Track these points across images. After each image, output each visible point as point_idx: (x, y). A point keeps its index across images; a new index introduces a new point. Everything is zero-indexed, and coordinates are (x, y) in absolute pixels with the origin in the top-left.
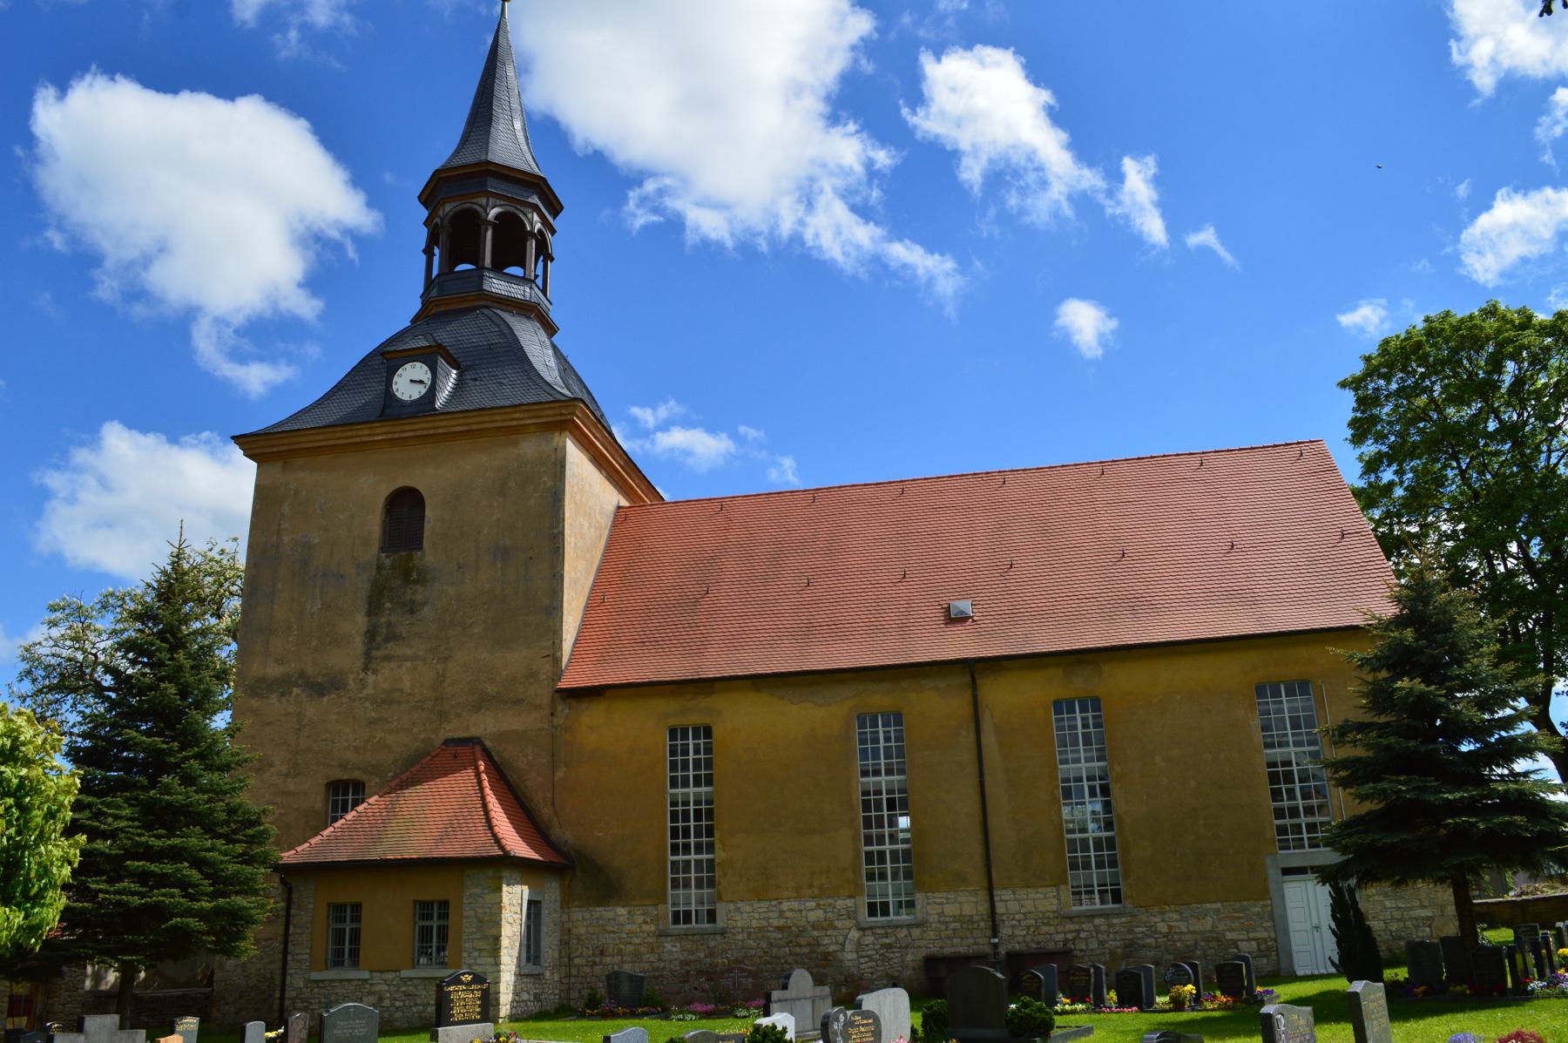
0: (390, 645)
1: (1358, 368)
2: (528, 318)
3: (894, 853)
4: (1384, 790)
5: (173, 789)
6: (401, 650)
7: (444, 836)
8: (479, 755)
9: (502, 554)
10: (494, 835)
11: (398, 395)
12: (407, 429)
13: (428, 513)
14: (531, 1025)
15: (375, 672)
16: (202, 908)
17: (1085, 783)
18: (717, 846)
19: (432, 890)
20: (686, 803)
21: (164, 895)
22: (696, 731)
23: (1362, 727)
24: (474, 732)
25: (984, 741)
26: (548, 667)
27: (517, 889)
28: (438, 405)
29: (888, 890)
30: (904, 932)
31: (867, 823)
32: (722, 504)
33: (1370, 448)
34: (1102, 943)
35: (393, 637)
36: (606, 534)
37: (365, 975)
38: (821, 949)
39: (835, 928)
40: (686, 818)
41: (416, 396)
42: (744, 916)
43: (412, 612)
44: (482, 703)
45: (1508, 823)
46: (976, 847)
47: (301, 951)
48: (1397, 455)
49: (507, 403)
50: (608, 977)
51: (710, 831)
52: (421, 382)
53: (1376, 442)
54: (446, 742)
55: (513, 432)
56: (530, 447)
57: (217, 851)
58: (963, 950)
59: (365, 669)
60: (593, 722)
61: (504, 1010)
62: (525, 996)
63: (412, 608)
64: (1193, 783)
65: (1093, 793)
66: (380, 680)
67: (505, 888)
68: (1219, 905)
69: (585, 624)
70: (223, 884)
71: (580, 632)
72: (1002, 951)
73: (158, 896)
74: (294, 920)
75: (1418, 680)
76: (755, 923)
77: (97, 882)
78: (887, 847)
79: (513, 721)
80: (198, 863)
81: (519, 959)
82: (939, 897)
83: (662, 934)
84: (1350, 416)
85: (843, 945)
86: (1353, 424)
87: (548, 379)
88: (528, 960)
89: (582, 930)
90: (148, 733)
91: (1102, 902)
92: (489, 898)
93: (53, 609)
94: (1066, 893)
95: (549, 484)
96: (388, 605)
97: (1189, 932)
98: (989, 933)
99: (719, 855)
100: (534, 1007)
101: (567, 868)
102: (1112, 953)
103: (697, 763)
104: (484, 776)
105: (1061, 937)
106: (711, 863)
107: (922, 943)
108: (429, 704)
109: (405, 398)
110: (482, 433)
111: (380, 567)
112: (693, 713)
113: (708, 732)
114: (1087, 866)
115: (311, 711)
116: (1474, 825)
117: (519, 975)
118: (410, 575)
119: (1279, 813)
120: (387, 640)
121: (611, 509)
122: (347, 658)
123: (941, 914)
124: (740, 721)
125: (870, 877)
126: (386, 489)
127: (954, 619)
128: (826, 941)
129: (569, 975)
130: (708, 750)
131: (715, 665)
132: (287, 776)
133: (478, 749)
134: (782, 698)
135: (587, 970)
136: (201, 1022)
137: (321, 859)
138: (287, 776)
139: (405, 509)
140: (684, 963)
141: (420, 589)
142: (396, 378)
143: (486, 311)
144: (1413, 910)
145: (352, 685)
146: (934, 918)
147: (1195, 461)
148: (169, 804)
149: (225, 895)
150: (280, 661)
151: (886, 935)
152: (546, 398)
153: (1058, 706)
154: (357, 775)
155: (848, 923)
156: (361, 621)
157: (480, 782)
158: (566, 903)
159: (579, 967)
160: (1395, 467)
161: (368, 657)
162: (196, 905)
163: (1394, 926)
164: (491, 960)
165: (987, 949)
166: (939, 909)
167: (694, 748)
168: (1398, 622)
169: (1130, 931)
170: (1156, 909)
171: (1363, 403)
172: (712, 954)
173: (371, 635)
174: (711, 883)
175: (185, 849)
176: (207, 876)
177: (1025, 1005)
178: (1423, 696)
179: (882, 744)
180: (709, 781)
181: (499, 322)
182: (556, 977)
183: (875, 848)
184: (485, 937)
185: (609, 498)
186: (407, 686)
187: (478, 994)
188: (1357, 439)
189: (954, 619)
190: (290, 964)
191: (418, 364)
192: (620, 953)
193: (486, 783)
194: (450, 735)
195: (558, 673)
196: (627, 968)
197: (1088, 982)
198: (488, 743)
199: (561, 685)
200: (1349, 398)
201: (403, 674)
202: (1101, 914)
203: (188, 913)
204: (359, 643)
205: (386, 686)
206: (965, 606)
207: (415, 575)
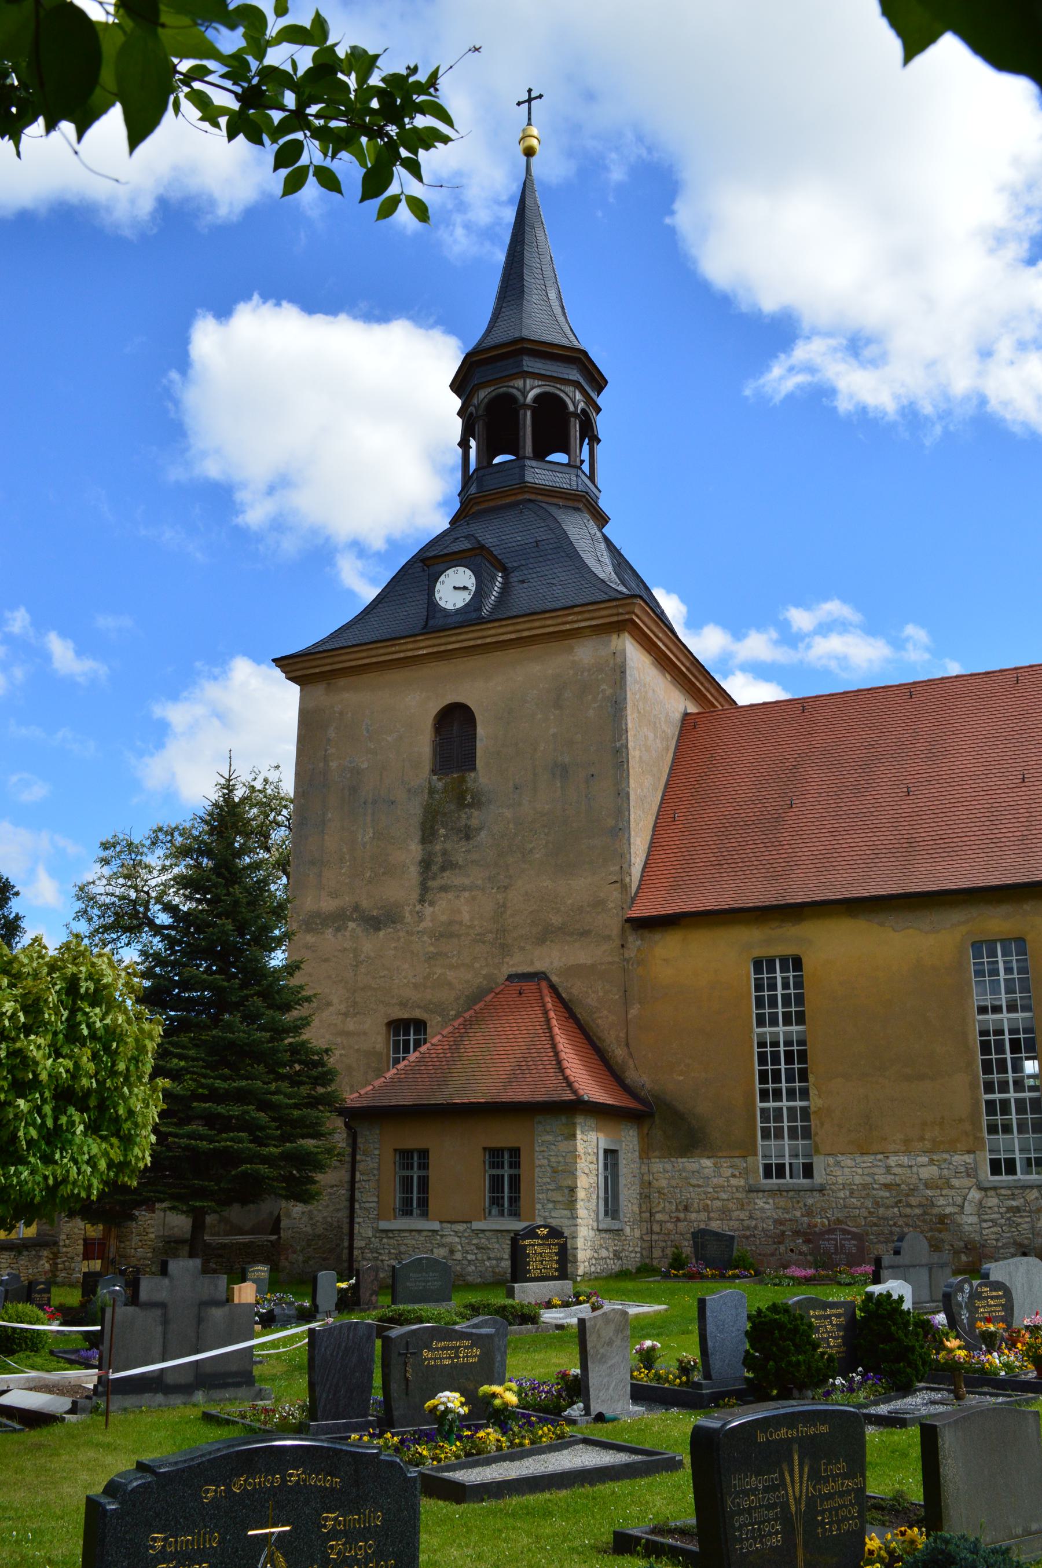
0: (447, 874)
6: (458, 881)
9: (562, 771)
10: (566, 1078)
11: (442, 604)
15: (432, 904)
18: (812, 1092)
19: (504, 1135)
20: (1000, 1032)
21: (232, 1140)
22: (784, 961)
24: (538, 966)
26: (616, 895)
27: (592, 1136)
37: (436, 1226)
39: (951, 1187)
40: (776, 1060)
41: (460, 604)
43: (468, 838)
44: (546, 935)
47: (367, 1198)
51: (804, 1076)
52: (465, 588)
54: (510, 978)
56: (586, 653)
57: (282, 1094)
59: (422, 901)
62: (604, 1253)
66: (438, 911)
67: (579, 1136)
74: (360, 1167)
76: (858, 1180)
78: (1012, 1095)
79: (582, 955)
83: (752, 1190)
89: (664, 1183)
92: (563, 1146)
95: (609, 692)
96: (442, 831)
99: (815, 1102)
103: (786, 999)
106: (805, 1111)
108: (490, 937)
109: (449, 606)
111: (432, 791)
112: (782, 939)
113: (797, 963)
115: (368, 945)
118: (464, 798)
120: (443, 869)
121: (677, 716)
122: (401, 889)
125: (992, 1129)
129: (652, 1232)
130: (799, 984)
132: (346, 1015)
134: (881, 924)
135: (670, 1226)
137: (386, 1103)
138: (346, 1015)
139: (455, 724)
140: (778, 1222)
141: (476, 813)
142: (438, 586)
150: (334, 895)
151: (1013, 1197)
154: (418, 1014)
155: (967, 1182)
156: (415, 849)
158: (645, 1153)
159: (661, 1223)
161: (424, 888)
162: (265, 1151)
164: (567, 1213)
167: (782, 980)
172: (809, 1213)
173: (426, 864)
174: (807, 1133)
180: (801, 1019)
183: (997, 1096)
184: (559, 1188)
185: (675, 704)
186: (466, 917)
191: (461, 569)
192: (706, 1209)
194: (513, 970)
196: (715, 1226)
198: (554, 979)
201: (462, 905)
204: (414, 872)
205: (444, 918)
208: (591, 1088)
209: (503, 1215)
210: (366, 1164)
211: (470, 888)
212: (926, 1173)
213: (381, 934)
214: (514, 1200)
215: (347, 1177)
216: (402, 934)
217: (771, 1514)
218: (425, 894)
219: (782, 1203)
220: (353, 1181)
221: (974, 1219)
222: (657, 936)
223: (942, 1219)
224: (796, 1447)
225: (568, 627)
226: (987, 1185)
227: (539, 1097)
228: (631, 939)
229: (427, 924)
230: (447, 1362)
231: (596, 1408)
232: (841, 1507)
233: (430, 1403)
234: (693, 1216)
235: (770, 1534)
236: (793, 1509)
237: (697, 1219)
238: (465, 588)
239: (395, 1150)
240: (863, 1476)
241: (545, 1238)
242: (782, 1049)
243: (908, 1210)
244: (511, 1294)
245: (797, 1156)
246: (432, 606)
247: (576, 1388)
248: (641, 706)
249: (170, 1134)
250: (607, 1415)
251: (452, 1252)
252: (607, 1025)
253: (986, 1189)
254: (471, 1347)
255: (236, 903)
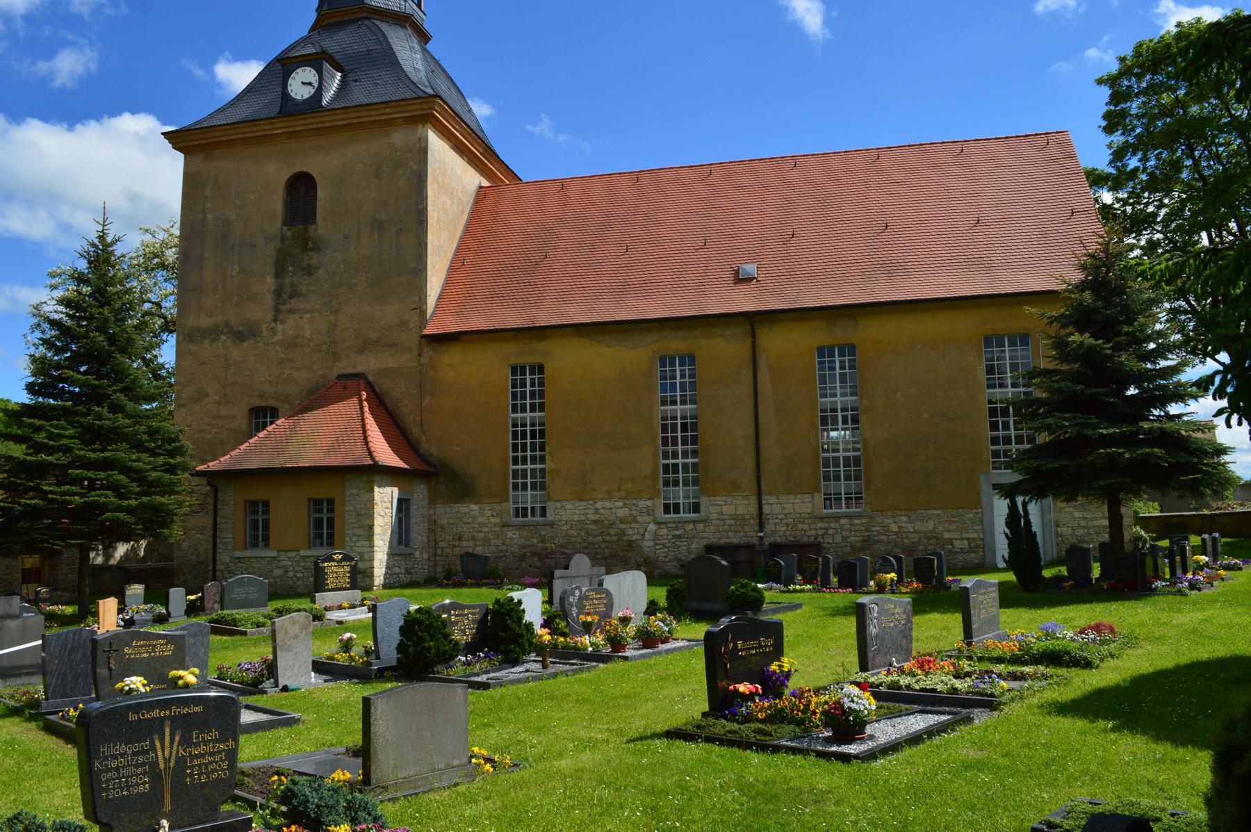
0: (293, 300)
1: (1114, 68)
2: (404, 27)
3: (685, 466)
4: (1050, 425)
5: (105, 417)
6: (302, 305)
7: (332, 448)
8: (362, 386)
9: (379, 226)
10: (369, 449)
11: (293, 95)
12: (299, 124)
13: (320, 193)
14: (398, 591)
15: (282, 322)
16: (130, 505)
17: (839, 413)
18: (548, 458)
19: (322, 490)
20: (524, 425)
21: (99, 496)
22: (532, 368)
23: (1047, 373)
24: (360, 369)
25: (760, 378)
26: (416, 318)
27: (388, 490)
28: (324, 102)
29: (681, 494)
30: (691, 526)
31: (665, 442)
32: (563, 184)
33: (1118, 138)
34: (845, 538)
35: (295, 294)
36: (468, 209)
37: (275, 554)
38: (626, 538)
39: (638, 522)
40: (524, 436)
41: (306, 96)
42: (568, 513)
43: (309, 274)
44: (365, 346)
45: (1147, 455)
46: (750, 463)
47: (226, 536)
48: (1141, 145)
49: (380, 100)
50: (462, 557)
51: (542, 449)
52: (310, 84)
53: (1123, 134)
54: (340, 377)
55: (385, 125)
56: (399, 137)
57: (142, 461)
58: (735, 541)
59: (275, 320)
60: (451, 360)
61: (379, 579)
62: (397, 570)
63: (309, 271)
64: (926, 415)
65: (845, 421)
66: (287, 328)
67: (376, 489)
68: (940, 512)
69: (448, 283)
70: (149, 487)
71: (444, 289)
72: (766, 542)
73: (94, 497)
74: (220, 513)
75: (1087, 335)
76: (576, 518)
77: (49, 485)
78: (680, 461)
79: (389, 361)
80: (126, 471)
81: (390, 542)
82: (718, 500)
83: (505, 525)
84: (1105, 109)
85: (643, 535)
86: (1107, 116)
87: (414, 79)
88: (400, 543)
89: (445, 521)
90: (84, 373)
91: (848, 507)
92: (365, 496)
93: (52, 275)
94: (819, 498)
95: (415, 168)
96: (291, 269)
97: (915, 532)
98: (757, 528)
99: (549, 465)
100: (405, 578)
101: (427, 473)
102: (853, 547)
103: (533, 394)
104: (365, 404)
105: (813, 533)
106: (543, 470)
107: (704, 535)
108: (324, 347)
109: (298, 97)
110: (361, 126)
111: (283, 238)
112: (529, 354)
113: (541, 369)
114: (837, 478)
115: (235, 353)
116: (1121, 454)
117: (391, 555)
118: (307, 244)
119: (995, 441)
120: (291, 297)
121: (472, 188)
122: (260, 311)
123: (720, 513)
124: (568, 363)
125: (666, 483)
126: (286, 174)
127: (741, 279)
128: (630, 532)
129: (435, 555)
130: (541, 384)
131: (546, 316)
132: (219, 403)
133: (362, 382)
134: (599, 342)
135: (449, 551)
136: (146, 589)
137: (237, 467)
138: (219, 403)
139: (301, 189)
140: (522, 547)
141: (315, 255)
142: (290, 81)
143: (367, 22)
144: (1066, 521)
145: (265, 332)
146: (714, 516)
147: (958, 148)
148: (101, 427)
149: (147, 494)
150: (210, 315)
151: (677, 528)
152: (411, 95)
153: (821, 350)
154: (272, 403)
155: (647, 519)
156: (270, 281)
157: (362, 408)
158: (433, 500)
159: (442, 548)
160: (1140, 155)
161: (277, 310)
162: (125, 503)
163: (1080, 532)
164: (367, 543)
165: (755, 541)
166: (718, 509)
167: (529, 381)
168: (1082, 287)
169: (868, 530)
170: (890, 513)
171: (1116, 98)
172: (543, 541)
173: (278, 292)
174: (543, 487)
175: (116, 460)
176: (133, 480)
177: (743, 586)
178: (1091, 348)
179: (678, 380)
180: (542, 407)
181: (376, 31)
182: (425, 556)
183: (671, 461)
184: (361, 526)
185: (473, 179)
186: (307, 333)
187: (348, 569)
188: (1109, 130)
189: (741, 279)
190: (219, 545)
191: (308, 69)
192: (474, 538)
193: (366, 409)
194: (341, 372)
195: (423, 322)
196: (479, 550)
197: (817, 569)
198: (371, 378)
199: (426, 332)
200: (1106, 92)
201: (305, 323)
202: (846, 516)
203: (119, 509)
204: (269, 299)
205: (291, 333)
206: (750, 268)
207: (311, 245)
208: (386, 455)
209: (322, 544)
210: (225, 511)
211: (311, 311)
212: (621, 513)
213: (245, 344)
214: (331, 536)
215: (211, 520)
216: (260, 344)
217: (139, 770)
218: (277, 316)
219: (525, 534)
220: (215, 524)
221: (650, 543)
222: (445, 348)
223: (630, 543)
224: (168, 723)
225: (386, 117)
226: (660, 520)
227: (348, 462)
228: (426, 350)
229: (279, 337)
230: (145, 655)
231: (282, 683)
232: (211, 763)
233: (119, 685)
234: (465, 543)
235: (137, 784)
236: (162, 766)
237: (467, 546)
238: (310, 84)
239: (246, 501)
240: (236, 740)
241: (340, 561)
242: (528, 428)
243: (608, 538)
244: (313, 601)
245: (688, 498)
246: (285, 95)
247: (271, 669)
248: (440, 179)
249: (51, 492)
250: (291, 687)
251: (286, 572)
252: (407, 412)
253: (659, 524)
254: (166, 644)
255: (106, 320)
